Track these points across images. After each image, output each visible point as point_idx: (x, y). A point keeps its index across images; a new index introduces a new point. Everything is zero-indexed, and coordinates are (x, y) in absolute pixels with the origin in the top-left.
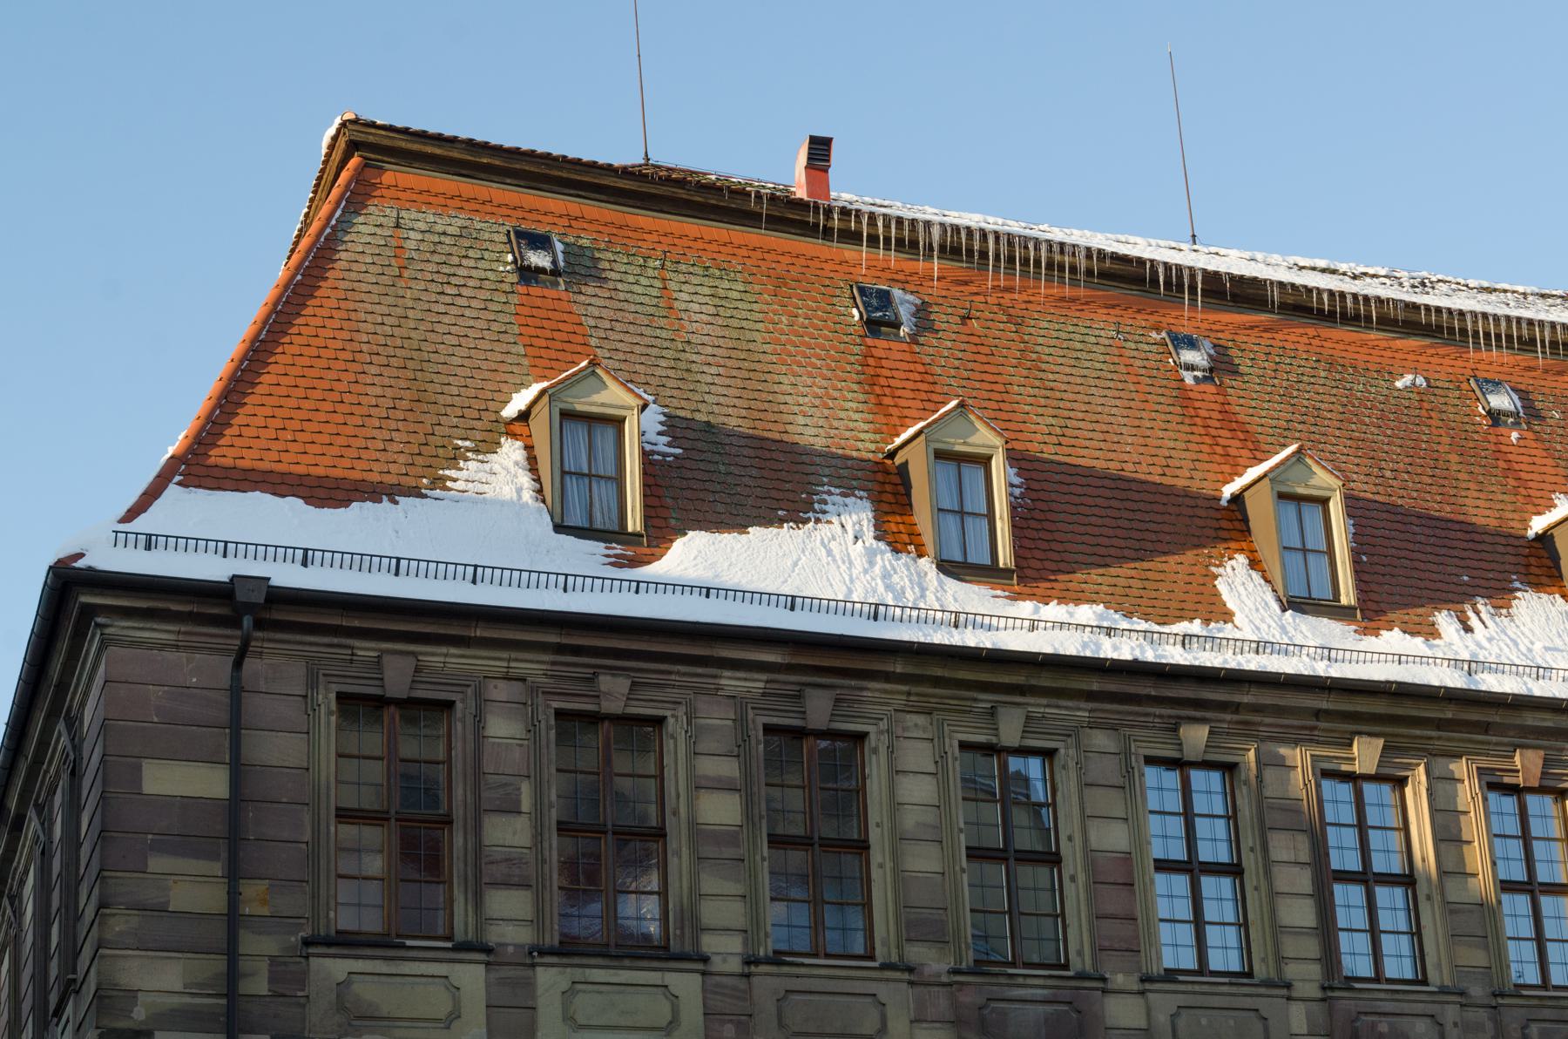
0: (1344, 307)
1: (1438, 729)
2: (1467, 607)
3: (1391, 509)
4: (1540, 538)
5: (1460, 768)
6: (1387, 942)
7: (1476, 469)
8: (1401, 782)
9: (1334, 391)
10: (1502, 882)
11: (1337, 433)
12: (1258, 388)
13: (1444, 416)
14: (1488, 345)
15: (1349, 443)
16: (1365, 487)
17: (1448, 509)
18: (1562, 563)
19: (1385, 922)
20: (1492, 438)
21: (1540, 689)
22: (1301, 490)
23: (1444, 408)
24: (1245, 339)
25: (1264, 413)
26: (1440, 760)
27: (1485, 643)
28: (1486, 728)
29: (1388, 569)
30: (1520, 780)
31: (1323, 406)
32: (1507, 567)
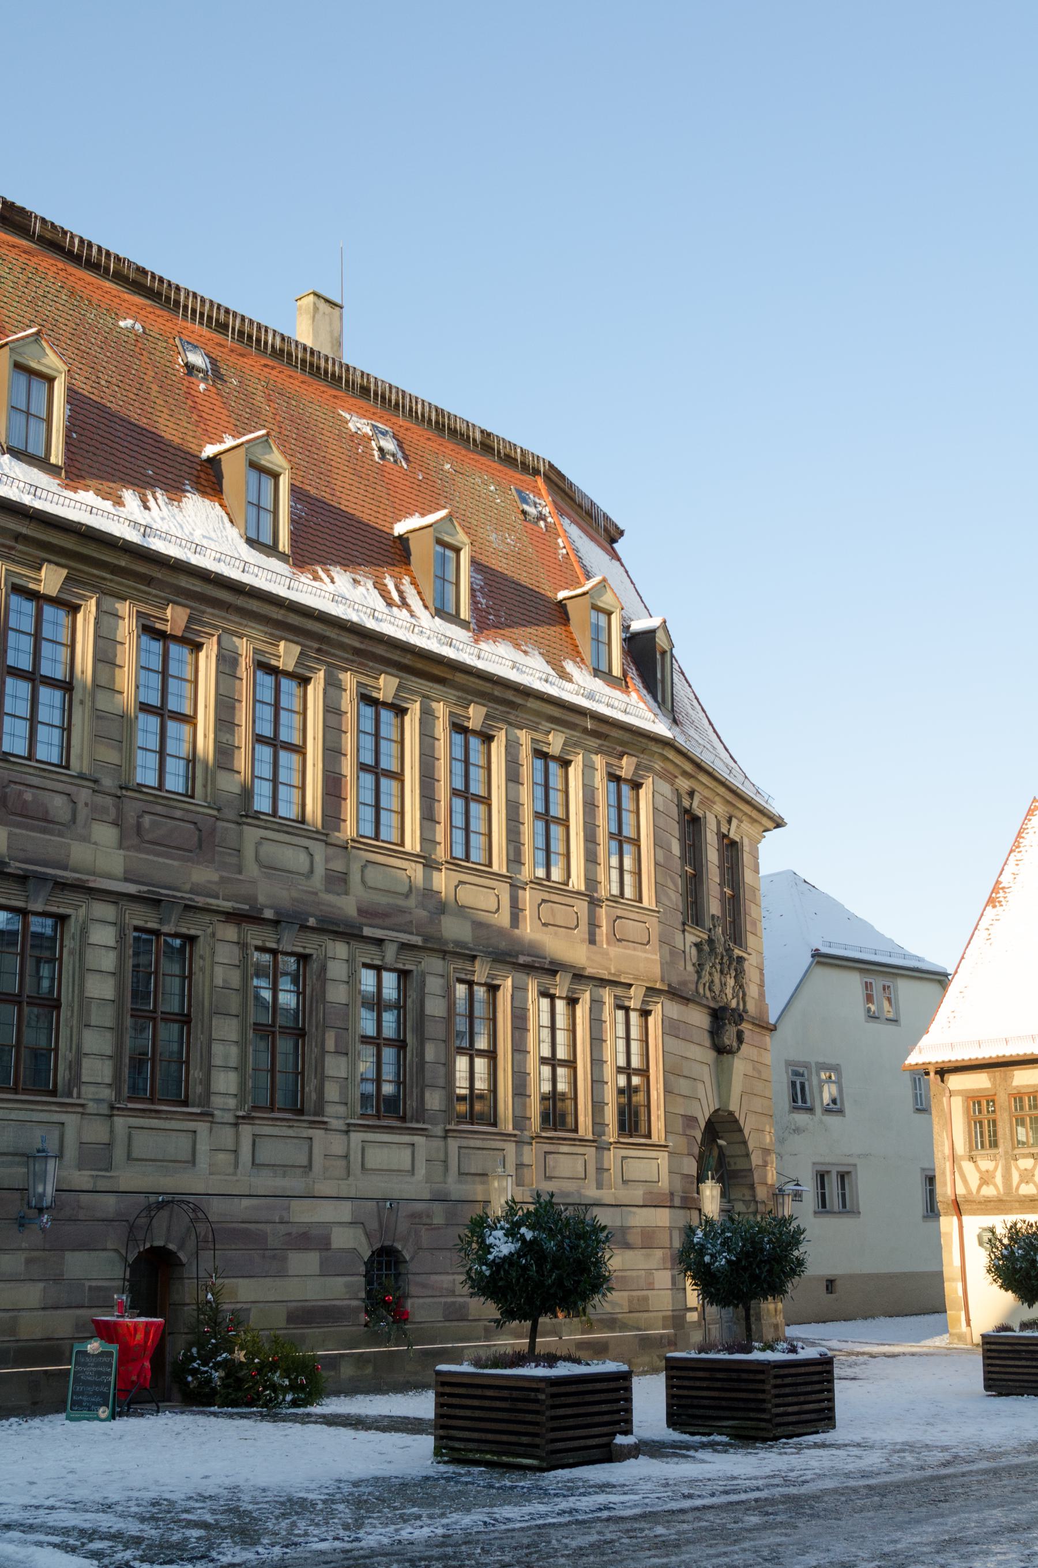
0: (89, 255)
1: (112, 573)
2: (149, 493)
3: (102, 408)
4: (209, 460)
5: (124, 608)
6: (42, 732)
7: (171, 400)
8: (74, 609)
9: (71, 312)
10: (141, 703)
11: (69, 342)
12: (11, 290)
13: (152, 357)
14: (193, 319)
15: (76, 351)
16: (84, 386)
17: (145, 420)
18: (224, 481)
19: (43, 715)
20: (186, 383)
21: (195, 560)
22: (34, 365)
23: (153, 351)
24: (7, 252)
25: (12, 309)
26: (108, 598)
27: (158, 520)
28: (149, 581)
29: (92, 449)
30: (168, 628)
31: (60, 320)
32: (183, 474)
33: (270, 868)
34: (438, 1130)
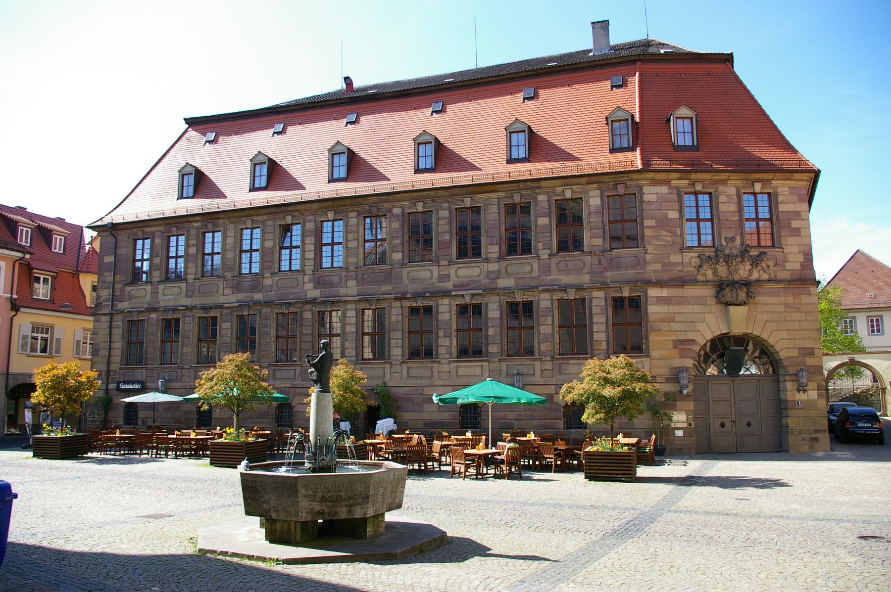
33: (413, 280)
34: (496, 360)
